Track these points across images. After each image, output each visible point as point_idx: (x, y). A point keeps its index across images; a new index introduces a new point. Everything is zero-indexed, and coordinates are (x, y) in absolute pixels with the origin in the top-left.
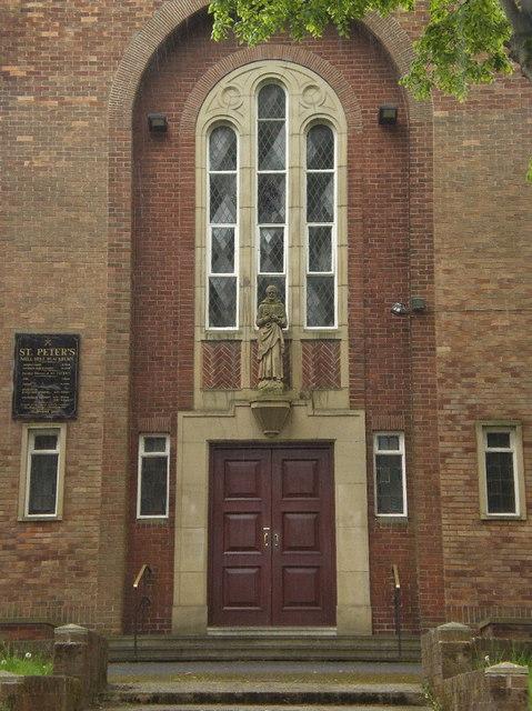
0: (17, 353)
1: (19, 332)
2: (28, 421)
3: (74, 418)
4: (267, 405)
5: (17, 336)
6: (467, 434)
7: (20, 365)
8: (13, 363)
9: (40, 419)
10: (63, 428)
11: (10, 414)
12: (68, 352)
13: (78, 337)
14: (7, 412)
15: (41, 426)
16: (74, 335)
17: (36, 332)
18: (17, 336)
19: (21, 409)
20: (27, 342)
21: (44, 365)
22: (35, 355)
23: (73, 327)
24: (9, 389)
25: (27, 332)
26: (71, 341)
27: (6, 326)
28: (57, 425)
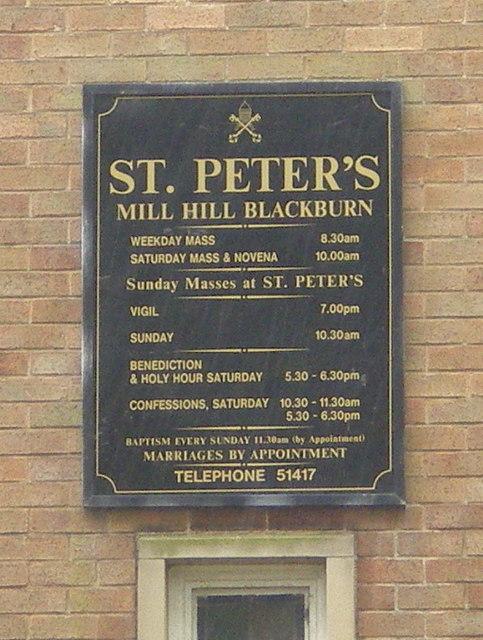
0: (99, 197)
1: (103, 75)
2: (164, 521)
3: (391, 510)
4: (277, 490)
5: (97, 98)
6: (209, 476)
7: (112, 241)
8: (77, 234)
9: (226, 512)
10: (338, 553)
11: (76, 491)
12: (346, 177)
13: (387, 93)
14: (57, 479)
15: (229, 546)
16: (397, 481)
17: (183, 72)
18: (97, 98)
19: (129, 464)
20: (144, 129)
21: (229, 242)
22: (188, 194)
23: (351, 57)
24: (62, 367)
25: (140, 73)
26: (354, 120)
27: (38, 48)
28: (302, 544)
